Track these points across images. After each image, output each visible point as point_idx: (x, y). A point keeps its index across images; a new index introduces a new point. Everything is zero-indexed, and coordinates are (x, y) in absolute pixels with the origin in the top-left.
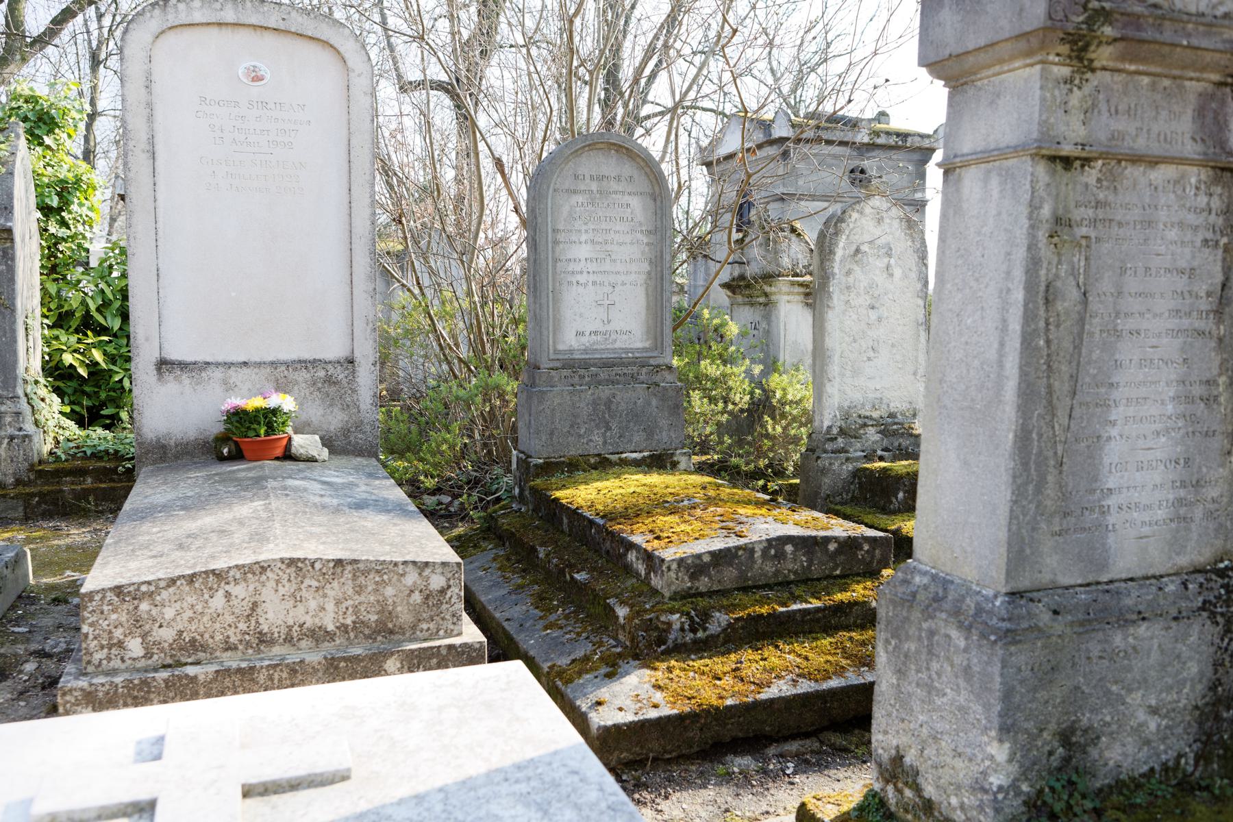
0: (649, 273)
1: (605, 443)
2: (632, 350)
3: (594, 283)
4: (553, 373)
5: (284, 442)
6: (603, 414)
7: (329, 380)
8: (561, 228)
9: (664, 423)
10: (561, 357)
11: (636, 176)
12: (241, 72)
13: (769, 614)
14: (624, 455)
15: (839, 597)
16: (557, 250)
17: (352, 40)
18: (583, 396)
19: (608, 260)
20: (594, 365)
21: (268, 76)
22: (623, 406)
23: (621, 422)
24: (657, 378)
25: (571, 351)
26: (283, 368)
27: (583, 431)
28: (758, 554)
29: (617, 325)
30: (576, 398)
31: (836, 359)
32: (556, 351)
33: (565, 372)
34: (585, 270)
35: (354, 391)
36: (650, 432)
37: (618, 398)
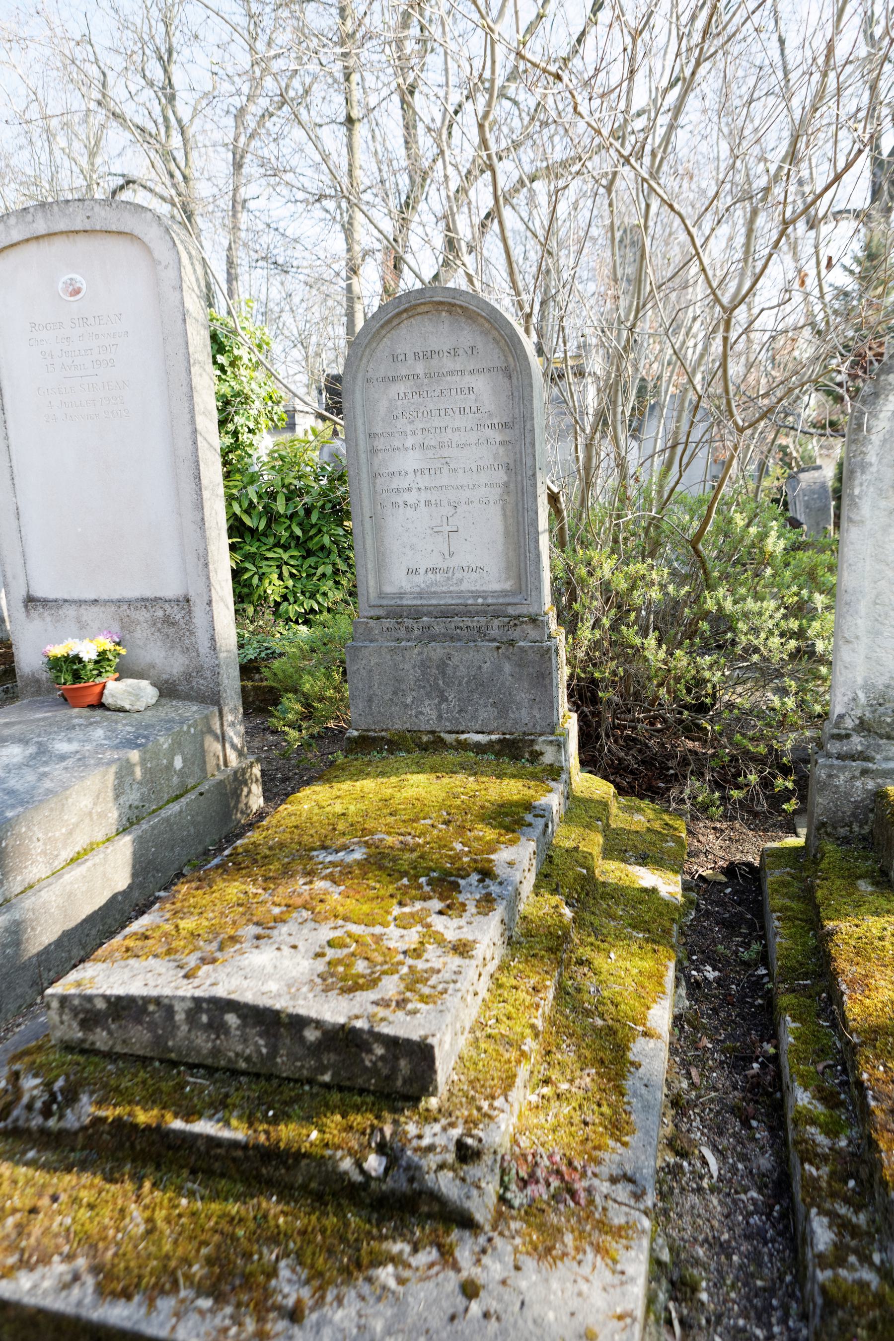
0: (506, 485)
1: (440, 717)
2: (484, 595)
3: (428, 503)
4: (372, 623)
5: (97, 689)
6: (436, 680)
7: (168, 621)
8: (379, 431)
9: (522, 697)
10: (385, 602)
11: (480, 346)
12: (61, 285)
13: (148, 1127)
14: (463, 737)
15: (287, 1133)
16: (376, 461)
17: (155, 226)
18: (407, 654)
19: (445, 470)
20: (429, 614)
21: (84, 288)
22: (462, 671)
23: (460, 692)
24: (515, 634)
25: (401, 595)
26: (125, 607)
27: (409, 701)
28: (180, 1017)
29: (464, 558)
30: (399, 658)
31: (863, 607)
32: (381, 595)
33: (387, 623)
34: (414, 486)
35: (192, 633)
36: (502, 709)
37: (456, 660)
